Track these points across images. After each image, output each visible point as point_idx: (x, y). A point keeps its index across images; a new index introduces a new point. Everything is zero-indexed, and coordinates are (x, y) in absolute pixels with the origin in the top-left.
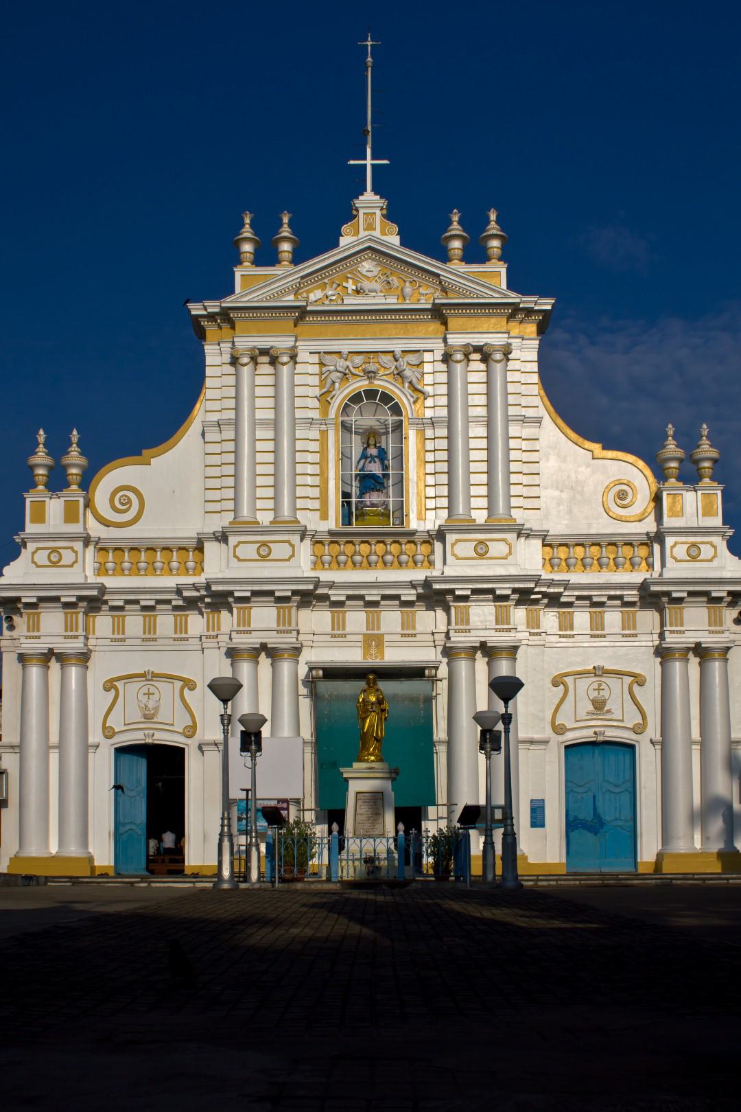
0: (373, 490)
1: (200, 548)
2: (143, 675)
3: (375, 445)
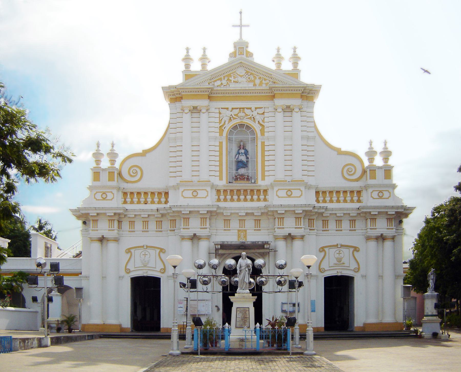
0: (242, 167)
3: (243, 148)
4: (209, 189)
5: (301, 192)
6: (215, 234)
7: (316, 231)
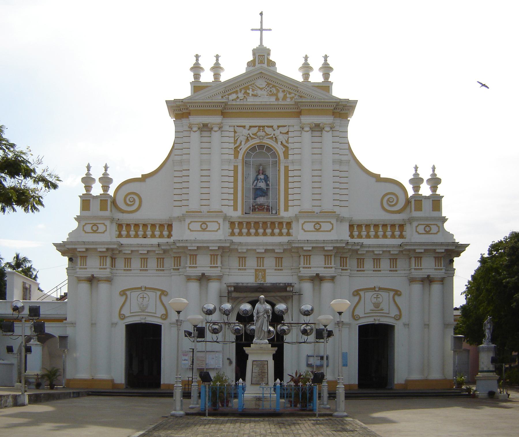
1: (170, 226)
2: (141, 288)
4: (221, 221)
5: (331, 226)
6: (228, 273)
7: (349, 271)
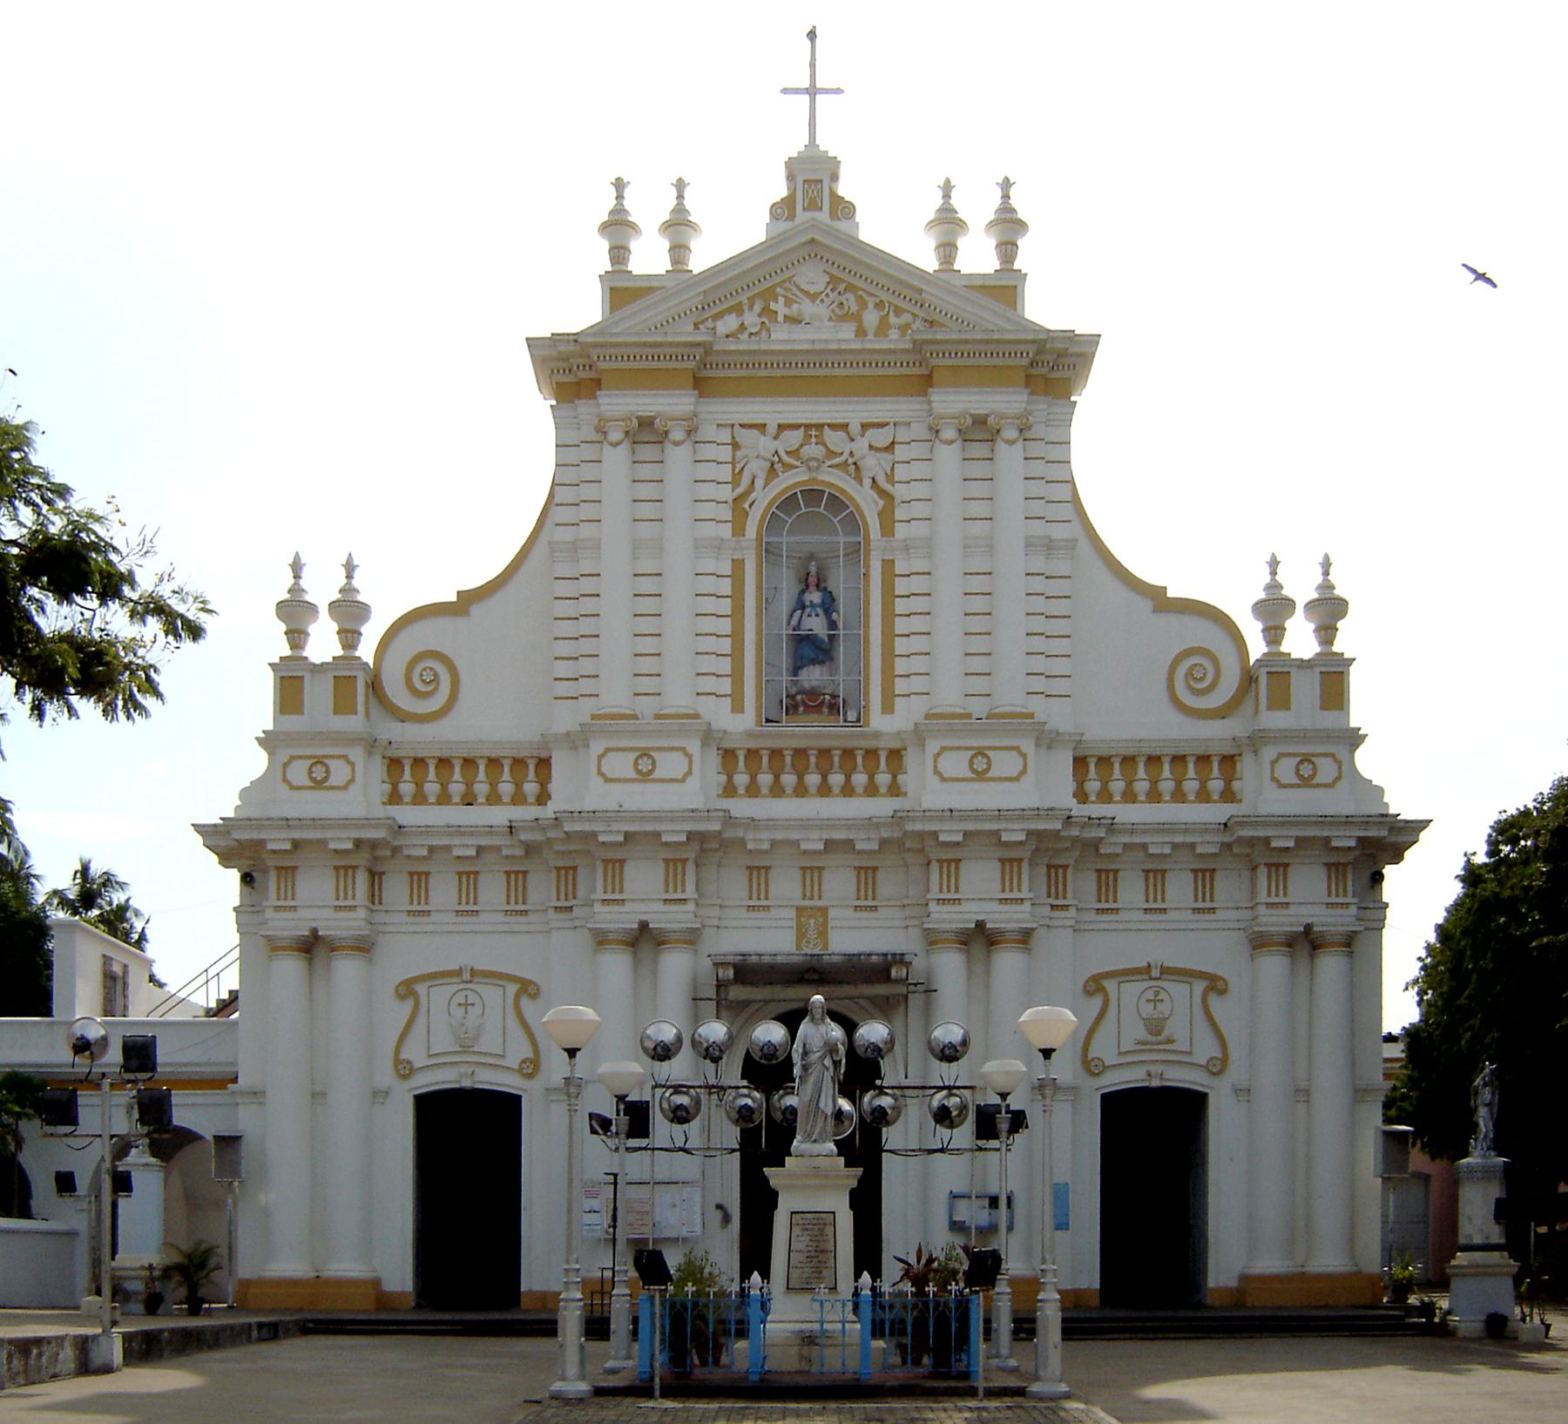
1: (544, 764)
6: (716, 922)
7: (1072, 912)
